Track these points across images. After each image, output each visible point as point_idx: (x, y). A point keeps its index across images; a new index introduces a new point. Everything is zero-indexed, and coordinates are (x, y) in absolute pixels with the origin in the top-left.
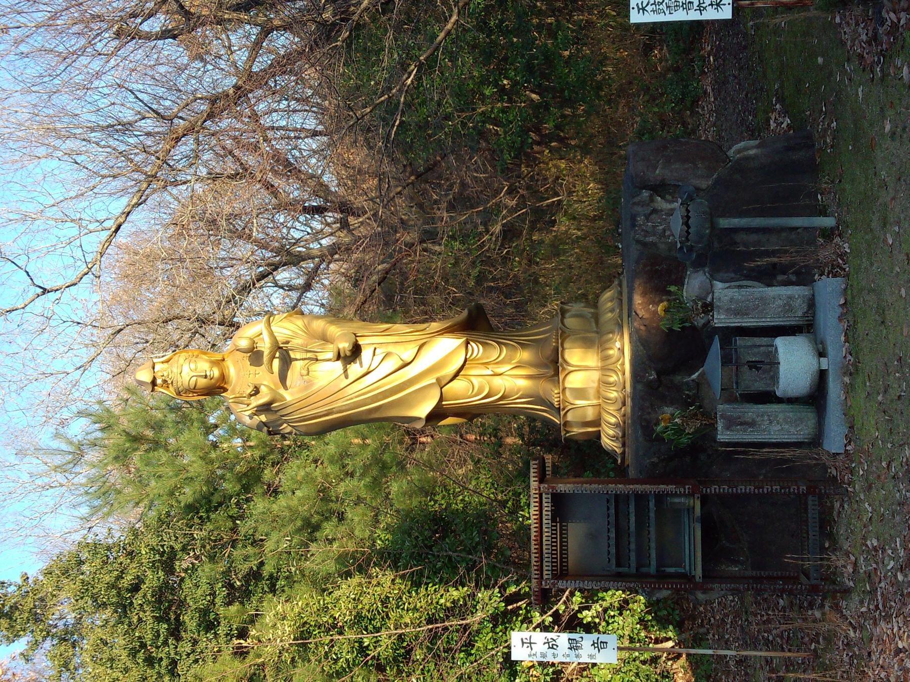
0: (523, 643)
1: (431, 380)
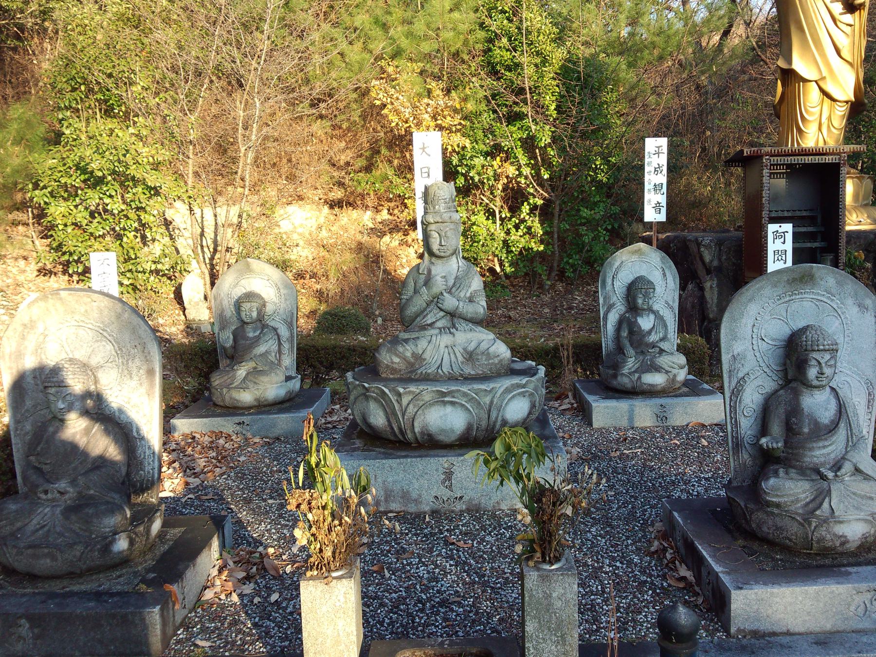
0: (659, 147)
1: (825, 73)
